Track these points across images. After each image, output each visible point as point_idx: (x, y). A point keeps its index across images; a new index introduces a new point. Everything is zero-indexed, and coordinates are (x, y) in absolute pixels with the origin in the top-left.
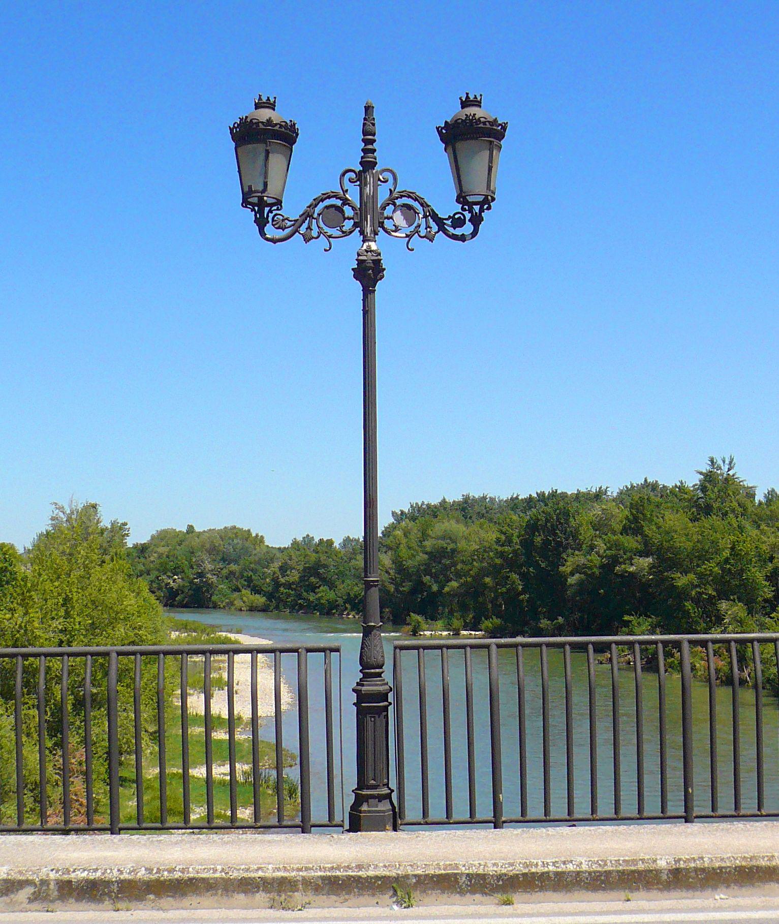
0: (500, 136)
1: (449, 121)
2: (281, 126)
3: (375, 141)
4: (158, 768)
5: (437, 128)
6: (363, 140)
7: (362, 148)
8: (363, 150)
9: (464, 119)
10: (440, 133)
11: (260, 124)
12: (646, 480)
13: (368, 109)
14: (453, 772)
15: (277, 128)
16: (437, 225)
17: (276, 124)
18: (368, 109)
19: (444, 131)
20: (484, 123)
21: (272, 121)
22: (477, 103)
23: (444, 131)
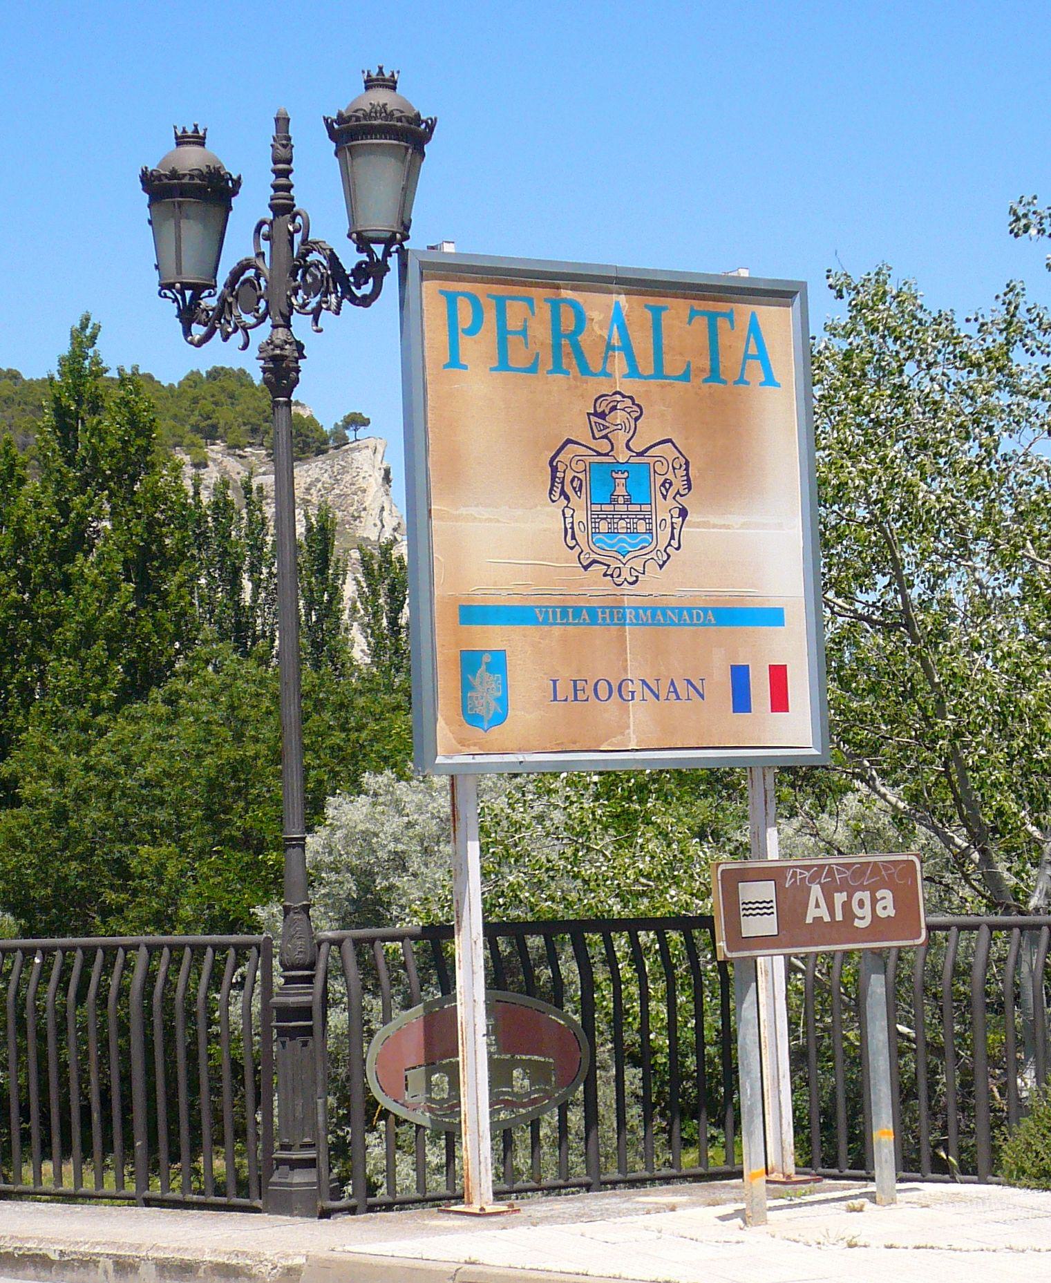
0: (426, 137)
1: (343, 110)
2: (192, 177)
3: (291, 171)
4: (214, 1167)
5: (326, 120)
6: (274, 171)
7: (271, 182)
8: (273, 186)
9: (368, 111)
10: (329, 127)
11: (163, 178)
12: (84, 336)
13: (282, 122)
14: (767, 1132)
15: (186, 180)
16: (373, 290)
17: (184, 175)
18: (282, 122)
19: (336, 126)
20: (399, 120)
21: (176, 172)
22: (391, 85)
23: (336, 126)
